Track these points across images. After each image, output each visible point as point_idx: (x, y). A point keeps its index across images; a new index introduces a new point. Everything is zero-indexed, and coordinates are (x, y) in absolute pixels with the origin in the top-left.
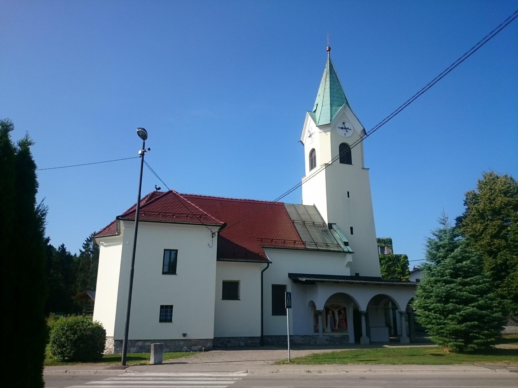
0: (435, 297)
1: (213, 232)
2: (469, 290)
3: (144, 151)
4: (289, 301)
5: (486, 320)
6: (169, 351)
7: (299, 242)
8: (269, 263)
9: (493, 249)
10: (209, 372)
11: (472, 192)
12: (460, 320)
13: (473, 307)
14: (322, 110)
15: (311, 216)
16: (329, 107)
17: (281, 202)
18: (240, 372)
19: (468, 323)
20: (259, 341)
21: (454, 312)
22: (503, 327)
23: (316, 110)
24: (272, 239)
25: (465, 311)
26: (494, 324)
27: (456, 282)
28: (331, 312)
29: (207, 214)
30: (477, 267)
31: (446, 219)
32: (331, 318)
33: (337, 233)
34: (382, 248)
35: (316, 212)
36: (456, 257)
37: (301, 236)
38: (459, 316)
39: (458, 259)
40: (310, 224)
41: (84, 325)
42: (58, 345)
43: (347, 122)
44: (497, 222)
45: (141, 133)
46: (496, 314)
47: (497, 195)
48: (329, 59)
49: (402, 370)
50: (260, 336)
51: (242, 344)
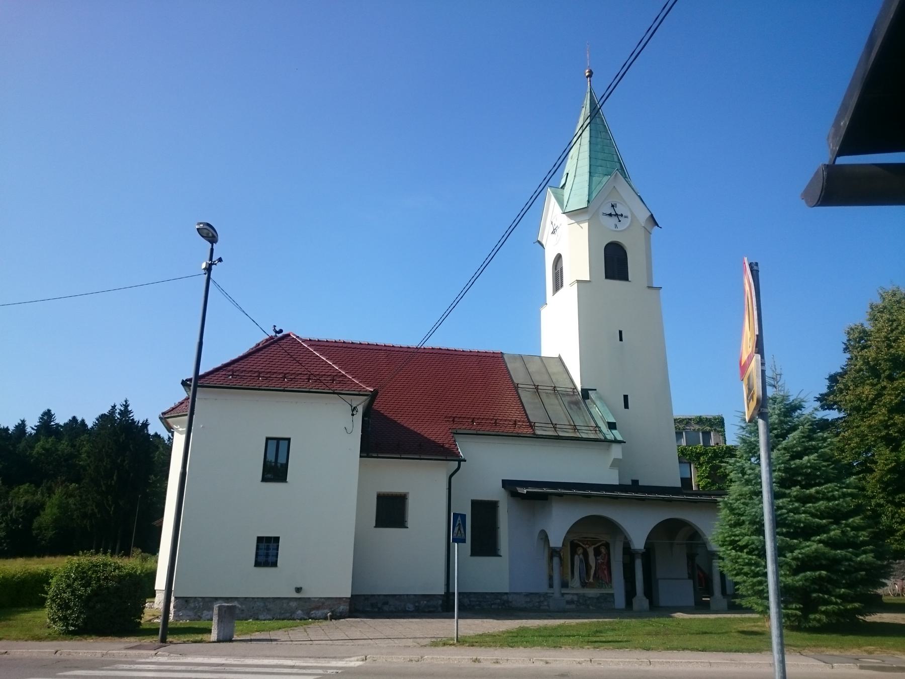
0: (749, 524)
1: (354, 406)
2: (813, 511)
3: (211, 263)
4: (459, 529)
5: (843, 569)
6: (271, 618)
7: (524, 422)
8: (460, 460)
9: (892, 433)
10: (300, 657)
11: (858, 326)
12: (795, 567)
13: (820, 541)
14: (574, 183)
15: (552, 377)
16: (586, 177)
17: (497, 352)
18: (353, 659)
19: (808, 573)
20: (440, 602)
21: (783, 553)
22: (884, 581)
23: (565, 184)
24: (474, 418)
25: (803, 551)
26: (859, 576)
27: (788, 496)
28: (580, 550)
29: (346, 375)
30: (831, 467)
31: (778, 376)
32: (581, 561)
33: (596, 406)
34: (707, 435)
35: (561, 369)
36: (792, 448)
37: (528, 412)
38: (792, 559)
39: (795, 452)
40: (547, 391)
41: (106, 571)
42: (59, 605)
43: (619, 202)
44: (901, 381)
45: (205, 231)
46: (862, 557)
47: (901, 332)
48: (589, 91)
49: (651, 660)
50: (444, 594)
51: (410, 607)
